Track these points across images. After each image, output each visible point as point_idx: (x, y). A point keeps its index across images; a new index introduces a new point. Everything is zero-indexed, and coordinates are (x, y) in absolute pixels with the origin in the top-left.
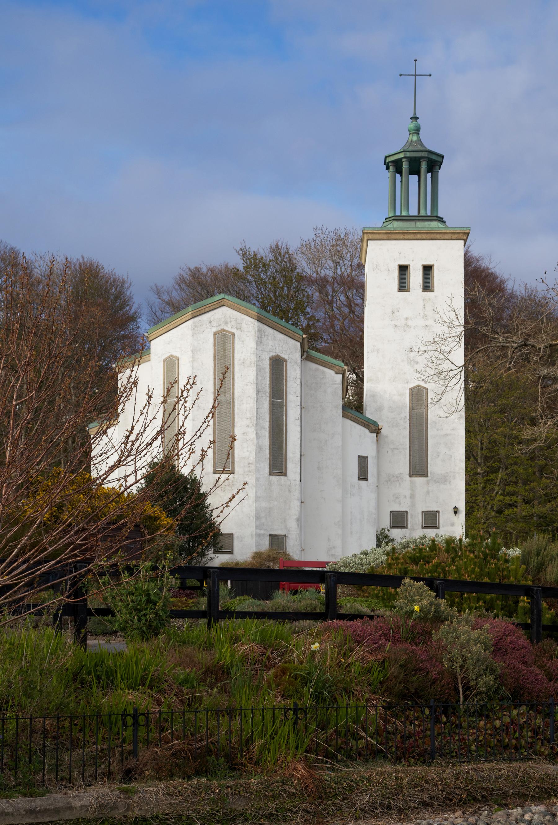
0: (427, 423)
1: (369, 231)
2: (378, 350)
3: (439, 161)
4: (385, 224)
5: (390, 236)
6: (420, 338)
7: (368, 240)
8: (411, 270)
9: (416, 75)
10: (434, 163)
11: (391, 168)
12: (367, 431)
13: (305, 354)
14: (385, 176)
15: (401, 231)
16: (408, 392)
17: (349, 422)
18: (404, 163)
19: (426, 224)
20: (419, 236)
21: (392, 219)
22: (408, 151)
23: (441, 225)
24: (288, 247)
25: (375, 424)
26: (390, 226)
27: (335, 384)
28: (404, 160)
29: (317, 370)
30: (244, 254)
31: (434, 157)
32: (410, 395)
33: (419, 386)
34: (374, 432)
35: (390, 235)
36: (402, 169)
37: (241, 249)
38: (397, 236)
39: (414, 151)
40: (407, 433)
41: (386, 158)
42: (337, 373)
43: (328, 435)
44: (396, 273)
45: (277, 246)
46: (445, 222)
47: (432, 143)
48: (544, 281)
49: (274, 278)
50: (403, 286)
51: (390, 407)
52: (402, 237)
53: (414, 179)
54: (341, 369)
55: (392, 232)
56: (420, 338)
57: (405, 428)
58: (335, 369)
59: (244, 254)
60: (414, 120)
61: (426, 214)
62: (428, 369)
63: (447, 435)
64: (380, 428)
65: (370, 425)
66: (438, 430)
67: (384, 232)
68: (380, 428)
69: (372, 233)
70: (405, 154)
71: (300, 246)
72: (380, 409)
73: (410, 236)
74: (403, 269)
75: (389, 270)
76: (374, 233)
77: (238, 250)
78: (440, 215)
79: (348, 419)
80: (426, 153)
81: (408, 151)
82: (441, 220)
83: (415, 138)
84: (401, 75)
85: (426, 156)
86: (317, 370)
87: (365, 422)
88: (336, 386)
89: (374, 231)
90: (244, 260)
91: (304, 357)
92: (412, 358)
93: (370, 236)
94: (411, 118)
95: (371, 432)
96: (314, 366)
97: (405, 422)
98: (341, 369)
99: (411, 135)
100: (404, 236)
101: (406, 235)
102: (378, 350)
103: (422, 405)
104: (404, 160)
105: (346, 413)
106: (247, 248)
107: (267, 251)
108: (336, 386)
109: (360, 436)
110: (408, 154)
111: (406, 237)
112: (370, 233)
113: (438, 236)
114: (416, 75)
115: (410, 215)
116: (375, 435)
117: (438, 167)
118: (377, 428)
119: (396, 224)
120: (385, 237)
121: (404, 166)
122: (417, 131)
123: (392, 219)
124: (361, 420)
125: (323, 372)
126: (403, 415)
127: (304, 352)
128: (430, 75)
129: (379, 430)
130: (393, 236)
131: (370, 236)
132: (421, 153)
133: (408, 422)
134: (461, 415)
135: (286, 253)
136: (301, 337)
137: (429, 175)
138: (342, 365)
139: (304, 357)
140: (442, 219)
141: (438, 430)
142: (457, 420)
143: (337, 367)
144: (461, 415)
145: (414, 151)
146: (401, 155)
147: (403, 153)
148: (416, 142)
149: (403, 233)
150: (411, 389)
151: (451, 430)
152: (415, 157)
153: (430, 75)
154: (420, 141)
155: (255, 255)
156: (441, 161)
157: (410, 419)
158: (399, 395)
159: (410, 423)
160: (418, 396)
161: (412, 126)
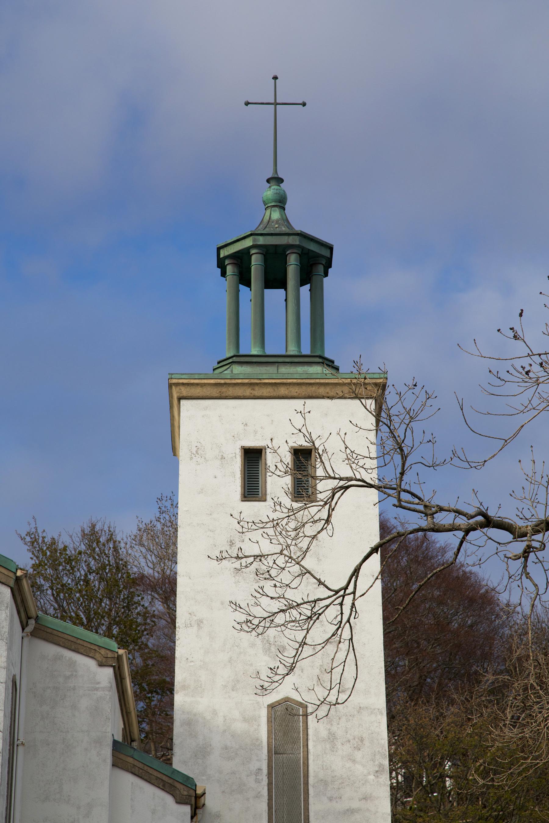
0: (306, 784)
1: (181, 381)
2: (200, 623)
3: (323, 256)
4: (217, 371)
5: (223, 391)
6: (236, 515)
7: (180, 399)
8: (270, 459)
9: (276, 104)
10: (315, 261)
11: (230, 269)
12: (169, 800)
13: (32, 622)
14: (218, 288)
15: (246, 381)
16: (264, 713)
17: (128, 780)
18: (253, 258)
19: (300, 369)
20: (283, 391)
21: (230, 360)
22: (261, 235)
23: (327, 371)
24: (112, 530)
25: (188, 782)
26: (228, 372)
27: (97, 689)
28: (253, 251)
29: (58, 658)
30: (34, 541)
31: (313, 247)
32: (269, 721)
33: (287, 700)
34: (186, 803)
35: (224, 389)
36: (251, 269)
37: (28, 534)
38: (239, 391)
39: (272, 235)
40: (263, 806)
41: (219, 249)
42: (101, 665)
43: (79, 808)
44: (237, 464)
45: (93, 526)
46: (337, 369)
47: (305, 218)
48: (520, 333)
49: (87, 582)
50: (252, 489)
51: (226, 748)
52: (248, 391)
53: (275, 296)
54: (110, 655)
55: (228, 381)
56: (236, 515)
57: (258, 796)
58: (97, 656)
59: (34, 541)
60: (273, 183)
61: (300, 352)
62: (264, 601)
63: (351, 811)
64: (199, 792)
65: (178, 785)
66: (330, 799)
67: (212, 381)
68: (199, 792)
69: (188, 384)
70: (254, 240)
71: (135, 531)
72: (203, 752)
73: (265, 391)
74: (253, 457)
75: (223, 458)
76: (192, 384)
77: (23, 535)
78: (327, 355)
79: (127, 770)
80: (297, 238)
81: (261, 235)
82: (330, 363)
83: (276, 215)
84: (247, 104)
85: (298, 243)
86: (58, 658)
87: (164, 778)
88: (99, 693)
89: (192, 381)
90: (33, 554)
91: (29, 629)
92: (272, 640)
93: (185, 391)
94: (268, 181)
95: (180, 801)
96: (51, 650)
97: (258, 781)
98: (110, 655)
99: (268, 212)
100: (253, 391)
101: (257, 388)
102: (200, 623)
103: (295, 741)
104: (253, 251)
105: (122, 756)
106: (40, 531)
107: (77, 539)
108: (99, 693)
109: (154, 812)
110: (261, 241)
111: (258, 391)
112: (183, 384)
113: (322, 391)
114: (276, 104)
115: (268, 352)
116: (187, 809)
117: (321, 268)
118: (192, 793)
119: (237, 369)
120: (214, 392)
121: (253, 263)
122: (281, 202)
123: (230, 360)
124: (155, 773)
125: (72, 664)
126: (254, 766)
127: (29, 618)
128: (304, 104)
129: (198, 797)
130: (231, 391)
131: (185, 391)
132: (286, 237)
133: (265, 781)
134: (381, 765)
135: (108, 541)
136: (11, 575)
137: (305, 290)
138: (113, 645)
139: (29, 629)
140: (333, 362)
141: (330, 799)
142: (371, 777)
143: (103, 651)
144: (381, 765)
145: (272, 235)
146: (248, 243)
147: (251, 238)
148: (277, 222)
149: (251, 384)
150: (271, 707)
151: (360, 800)
152: (276, 246)
153: (304, 104)
154: (286, 221)
155: (54, 542)
156: (328, 255)
157: (270, 774)
158: (245, 720)
159: (270, 784)
160: (287, 719)
161: (270, 193)
